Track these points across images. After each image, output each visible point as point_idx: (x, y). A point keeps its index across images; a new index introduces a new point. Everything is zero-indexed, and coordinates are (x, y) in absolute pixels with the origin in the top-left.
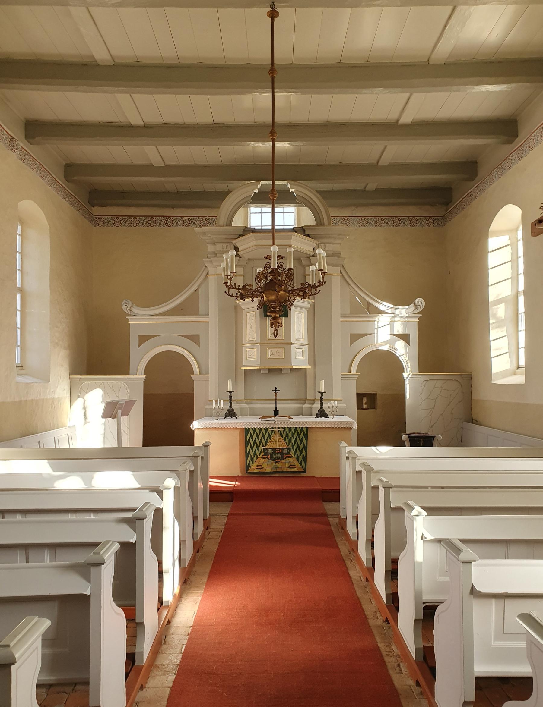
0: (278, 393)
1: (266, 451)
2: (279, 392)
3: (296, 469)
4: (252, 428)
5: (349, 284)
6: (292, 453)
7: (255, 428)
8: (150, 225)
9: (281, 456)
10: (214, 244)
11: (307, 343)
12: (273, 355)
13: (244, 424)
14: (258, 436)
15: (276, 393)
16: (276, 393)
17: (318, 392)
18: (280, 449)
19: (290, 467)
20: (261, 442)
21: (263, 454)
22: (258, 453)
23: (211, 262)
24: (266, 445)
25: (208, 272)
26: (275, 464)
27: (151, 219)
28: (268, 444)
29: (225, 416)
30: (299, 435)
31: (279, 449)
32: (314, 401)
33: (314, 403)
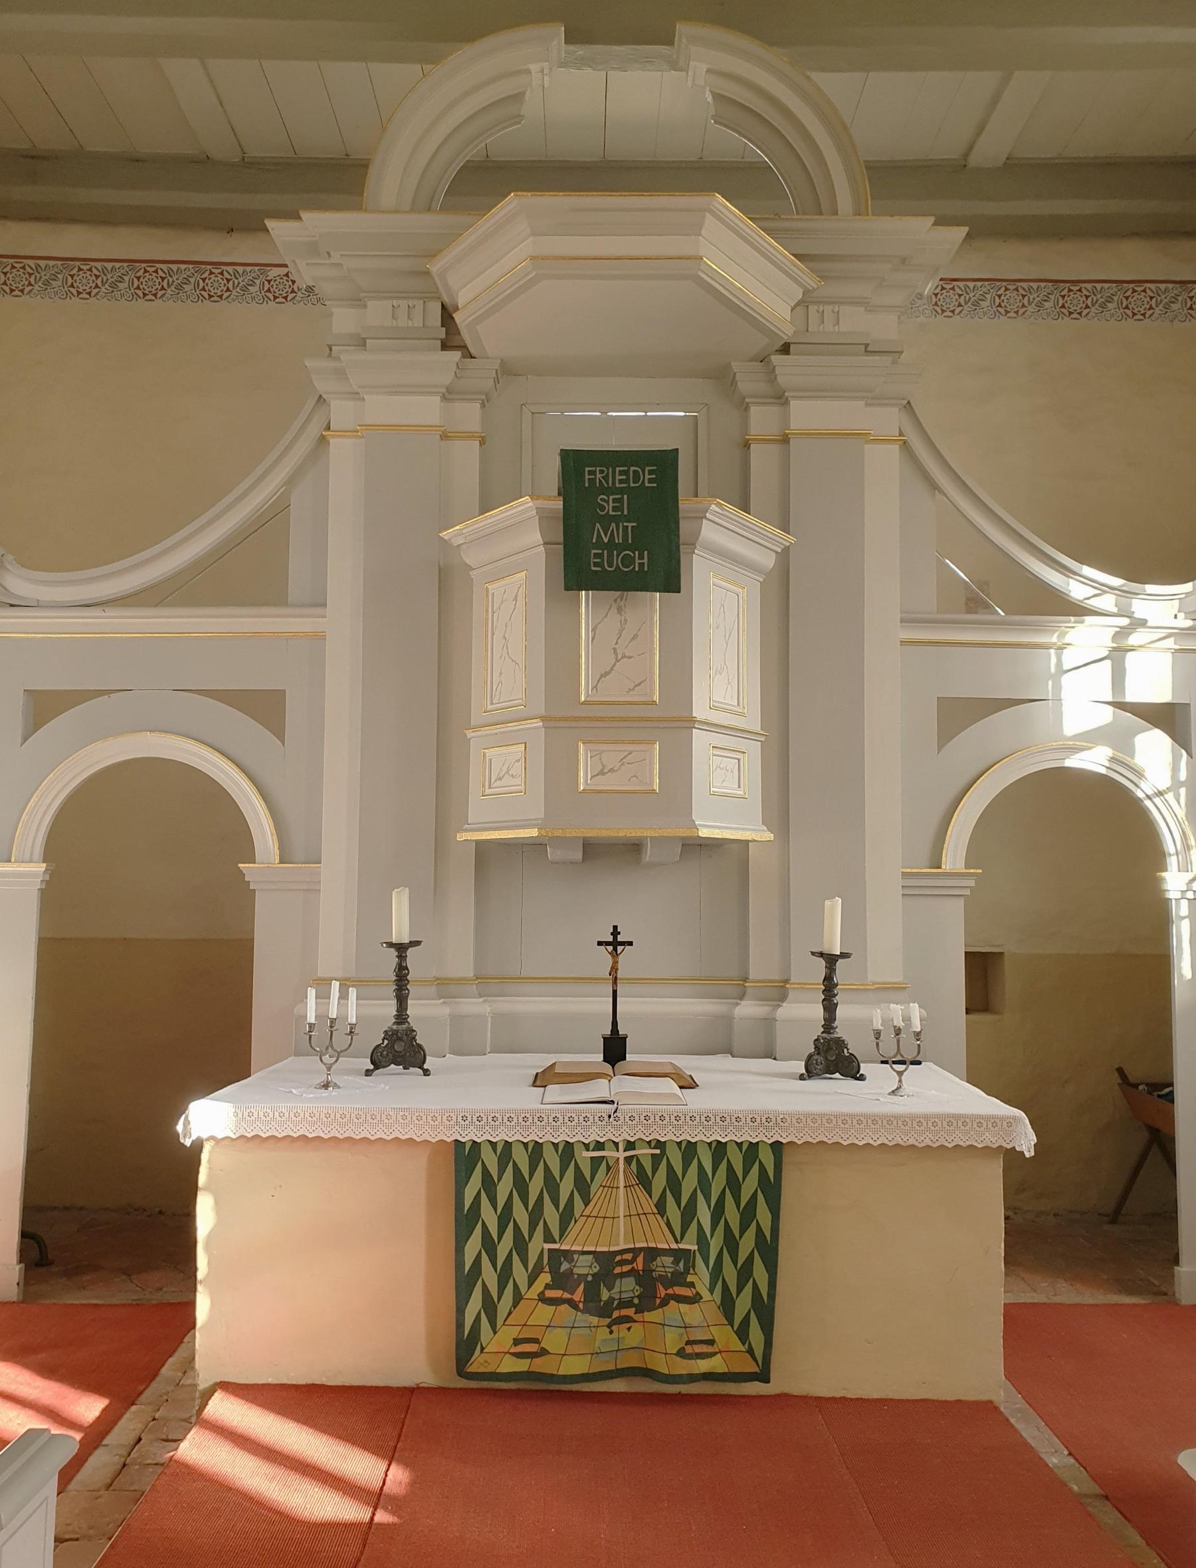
0: (626, 953)
1: (565, 1266)
2: (628, 947)
3: (715, 1364)
4: (493, 1145)
5: (934, 487)
6: (701, 1276)
7: (508, 1145)
8: (140, 293)
9: (638, 1290)
10: (357, 301)
11: (758, 729)
12: (604, 774)
13: (449, 1119)
14: (521, 1185)
15: (615, 954)
16: (615, 954)
17: (813, 953)
18: (635, 1251)
19: (689, 1349)
20: (536, 1216)
21: (545, 1278)
22: (520, 1273)
23: (341, 374)
24: (561, 1237)
25: (329, 422)
26: (611, 1332)
27: (146, 271)
28: (574, 1229)
29: (372, 1062)
30: (734, 1184)
31: (629, 1256)
32: (780, 991)
33: (783, 998)
